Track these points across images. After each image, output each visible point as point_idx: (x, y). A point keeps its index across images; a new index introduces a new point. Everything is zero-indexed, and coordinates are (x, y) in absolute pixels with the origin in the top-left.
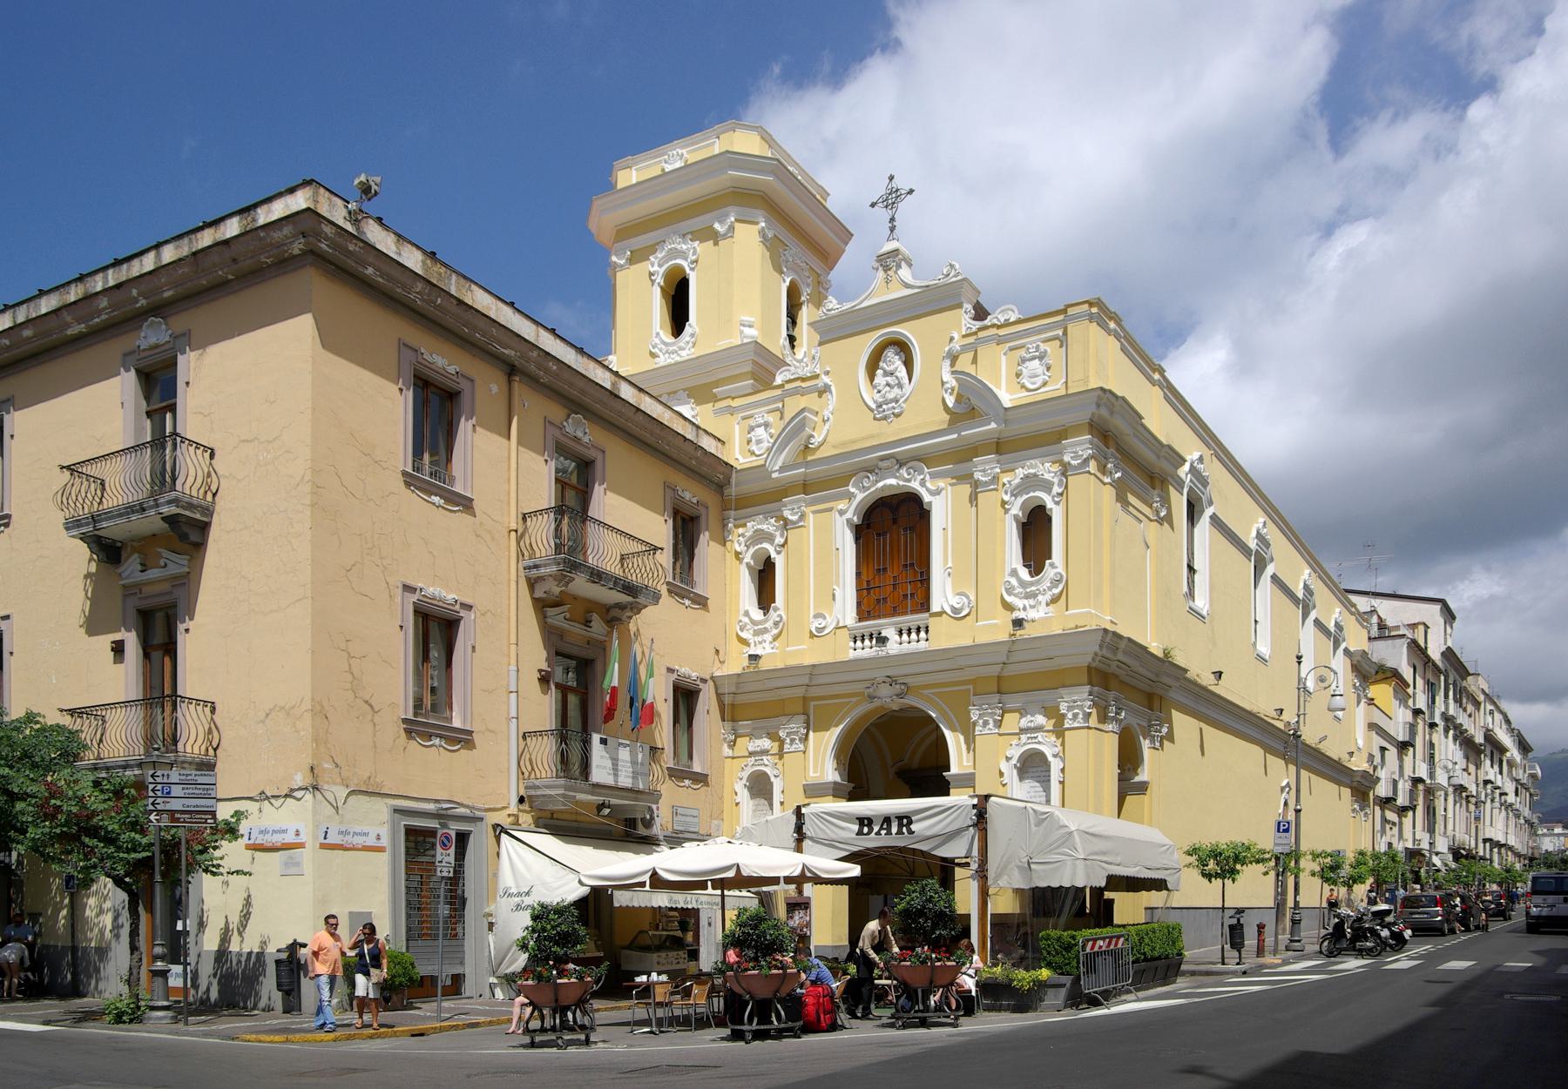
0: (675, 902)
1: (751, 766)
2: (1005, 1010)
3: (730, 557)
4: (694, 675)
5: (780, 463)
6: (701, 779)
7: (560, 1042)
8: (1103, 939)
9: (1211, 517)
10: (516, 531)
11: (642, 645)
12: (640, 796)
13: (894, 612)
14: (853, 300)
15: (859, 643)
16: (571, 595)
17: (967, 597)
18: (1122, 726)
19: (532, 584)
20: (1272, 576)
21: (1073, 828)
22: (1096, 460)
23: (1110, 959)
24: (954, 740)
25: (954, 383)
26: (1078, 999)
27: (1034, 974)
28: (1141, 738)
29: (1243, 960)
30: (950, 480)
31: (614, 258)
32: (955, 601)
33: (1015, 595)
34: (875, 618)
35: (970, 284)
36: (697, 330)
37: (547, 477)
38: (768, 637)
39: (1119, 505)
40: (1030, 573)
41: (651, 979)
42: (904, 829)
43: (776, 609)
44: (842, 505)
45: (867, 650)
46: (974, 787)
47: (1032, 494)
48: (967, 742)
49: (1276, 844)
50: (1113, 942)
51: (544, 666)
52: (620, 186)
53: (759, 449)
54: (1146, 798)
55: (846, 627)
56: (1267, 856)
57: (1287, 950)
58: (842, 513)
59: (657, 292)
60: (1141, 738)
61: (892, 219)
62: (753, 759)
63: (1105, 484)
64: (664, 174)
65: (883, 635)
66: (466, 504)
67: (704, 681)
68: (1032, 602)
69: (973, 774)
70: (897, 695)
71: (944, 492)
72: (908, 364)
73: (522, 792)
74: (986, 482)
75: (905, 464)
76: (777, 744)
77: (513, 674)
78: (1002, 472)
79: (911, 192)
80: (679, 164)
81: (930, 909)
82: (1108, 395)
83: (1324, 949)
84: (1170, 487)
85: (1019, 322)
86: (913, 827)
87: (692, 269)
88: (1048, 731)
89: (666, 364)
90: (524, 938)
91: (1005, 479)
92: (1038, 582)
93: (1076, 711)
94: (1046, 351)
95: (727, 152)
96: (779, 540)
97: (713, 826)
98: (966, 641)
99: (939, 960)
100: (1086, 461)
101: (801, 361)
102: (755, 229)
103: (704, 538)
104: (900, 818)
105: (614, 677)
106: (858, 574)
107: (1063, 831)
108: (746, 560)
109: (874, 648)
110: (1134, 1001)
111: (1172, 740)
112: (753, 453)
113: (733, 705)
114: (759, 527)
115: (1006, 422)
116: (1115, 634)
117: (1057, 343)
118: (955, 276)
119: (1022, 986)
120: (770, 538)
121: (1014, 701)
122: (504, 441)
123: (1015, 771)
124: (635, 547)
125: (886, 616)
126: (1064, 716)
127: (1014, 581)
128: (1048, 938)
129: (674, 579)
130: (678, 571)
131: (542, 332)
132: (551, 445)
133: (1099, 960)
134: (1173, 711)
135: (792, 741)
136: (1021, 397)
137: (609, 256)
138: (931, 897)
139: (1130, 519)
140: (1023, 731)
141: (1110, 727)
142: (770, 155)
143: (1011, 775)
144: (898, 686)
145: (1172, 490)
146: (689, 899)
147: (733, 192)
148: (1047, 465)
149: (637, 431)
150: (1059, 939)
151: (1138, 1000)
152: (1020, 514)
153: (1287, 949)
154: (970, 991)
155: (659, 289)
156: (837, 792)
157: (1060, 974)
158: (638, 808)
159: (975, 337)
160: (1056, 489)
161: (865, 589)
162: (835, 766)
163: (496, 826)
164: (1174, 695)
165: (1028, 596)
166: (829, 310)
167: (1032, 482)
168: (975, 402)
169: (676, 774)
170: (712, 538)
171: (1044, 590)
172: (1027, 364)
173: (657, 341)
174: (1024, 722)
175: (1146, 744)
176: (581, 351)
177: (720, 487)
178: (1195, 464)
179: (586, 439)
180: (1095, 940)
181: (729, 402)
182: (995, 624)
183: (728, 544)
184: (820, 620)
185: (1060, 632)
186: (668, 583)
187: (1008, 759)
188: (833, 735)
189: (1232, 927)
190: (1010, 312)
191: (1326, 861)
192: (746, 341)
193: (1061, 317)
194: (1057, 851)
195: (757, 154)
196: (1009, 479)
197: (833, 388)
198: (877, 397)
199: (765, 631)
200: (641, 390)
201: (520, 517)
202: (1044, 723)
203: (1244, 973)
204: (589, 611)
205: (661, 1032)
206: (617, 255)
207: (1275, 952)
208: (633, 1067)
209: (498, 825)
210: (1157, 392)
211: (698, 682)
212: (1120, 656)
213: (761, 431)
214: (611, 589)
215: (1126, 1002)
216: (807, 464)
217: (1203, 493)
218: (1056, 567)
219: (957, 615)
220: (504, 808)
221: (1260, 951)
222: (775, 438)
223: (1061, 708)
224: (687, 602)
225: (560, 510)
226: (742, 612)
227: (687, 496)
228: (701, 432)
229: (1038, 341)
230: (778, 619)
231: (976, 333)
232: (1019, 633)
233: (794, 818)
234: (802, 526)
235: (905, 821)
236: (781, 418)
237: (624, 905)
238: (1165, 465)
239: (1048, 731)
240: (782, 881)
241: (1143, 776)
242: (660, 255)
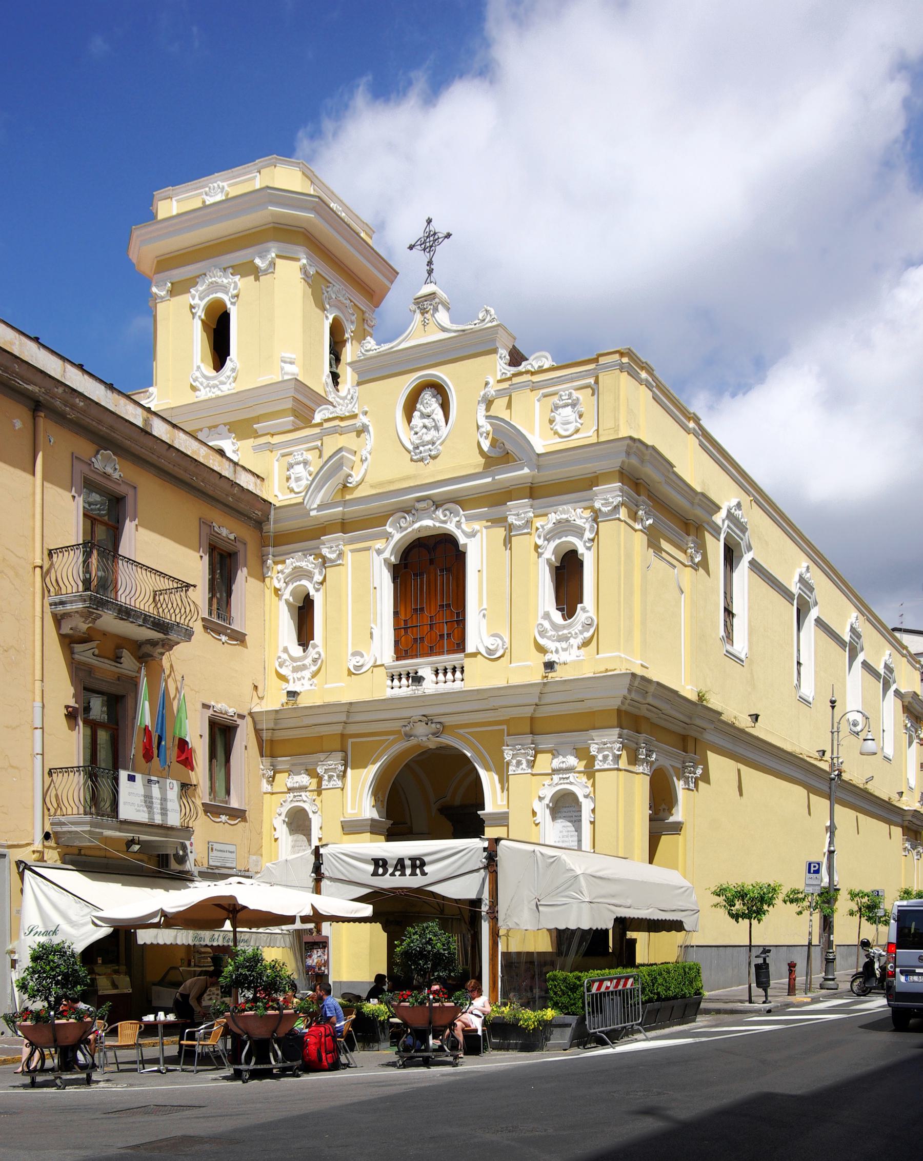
0: (200, 940)
1: (289, 803)
2: (513, 1049)
3: (269, 594)
4: (231, 711)
5: (318, 502)
6: (239, 815)
7: (58, 1081)
8: (611, 980)
9: (750, 562)
10: (41, 567)
11: (176, 681)
12: (170, 832)
13: (431, 652)
14: (390, 341)
15: (396, 682)
16: (99, 631)
17: (502, 639)
18: (654, 767)
19: (58, 620)
20: (816, 620)
21: (579, 872)
22: (626, 507)
23: (618, 999)
24: (488, 780)
25: (489, 428)
26: (582, 1039)
27: (539, 1013)
28: (675, 779)
29: (769, 999)
30: (484, 523)
31: (154, 290)
32: (491, 642)
33: (549, 638)
34: (412, 657)
35: (505, 329)
36: (238, 367)
37: (75, 512)
38: (307, 674)
39: (651, 550)
40: (563, 616)
41: (158, 1018)
42: (418, 871)
43: (315, 646)
44: (379, 544)
45: (404, 689)
46: (508, 826)
47: (564, 539)
48: (501, 782)
49: (807, 885)
50: (622, 983)
51: (72, 703)
52: (160, 216)
53: (299, 486)
54: (680, 838)
55: (383, 665)
56: (800, 896)
57: (821, 988)
58: (379, 552)
59: (198, 325)
60: (675, 779)
61: (430, 263)
62: (292, 795)
63: (636, 531)
64: (205, 206)
65: (419, 674)
66: (338, 390)
67: (242, 717)
68: (564, 645)
69: (507, 813)
70: (433, 734)
71: (479, 534)
72: (445, 406)
73: (48, 828)
74: (520, 526)
75: (441, 505)
76: (315, 781)
77: (38, 711)
78: (535, 516)
79: (448, 236)
80: (219, 197)
81: (429, 952)
82: (638, 444)
83: (855, 988)
84: (707, 534)
85: (552, 369)
86: (426, 869)
87: (233, 304)
88: (579, 772)
89: (206, 398)
90: (23, 979)
91: (538, 523)
92: (570, 626)
93: (606, 753)
94: (578, 399)
95: (268, 187)
96: (318, 578)
97: (251, 861)
98: (499, 682)
99: (437, 1001)
100: (616, 508)
101: (344, 398)
102: (296, 265)
103: (242, 574)
104: (413, 859)
105: (145, 715)
106: (396, 613)
107: (570, 874)
108: (285, 597)
109: (411, 687)
110: (644, 1040)
111: (708, 782)
112: (292, 491)
113: (272, 741)
114: (298, 564)
115: (539, 467)
116: (643, 678)
117: (589, 391)
118: (491, 321)
119: (528, 1025)
120: (309, 575)
121: (547, 742)
122: (29, 477)
123: (548, 811)
124: (166, 584)
125: (423, 655)
126: (594, 758)
127: (547, 624)
128: (554, 979)
129: (210, 614)
130: (215, 606)
131: (69, 367)
132: (79, 480)
133: (607, 1000)
134: (709, 753)
135: (330, 777)
136: (555, 444)
137: (150, 287)
138: (430, 939)
139: (663, 564)
140: (555, 771)
141: (640, 769)
142: (312, 192)
143: (544, 815)
144: (433, 725)
145: (707, 536)
146: (216, 936)
147: (274, 228)
148: (579, 511)
149: (169, 467)
150: (565, 980)
151: (647, 1039)
152: (553, 559)
153: (822, 987)
154: (476, 1030)
155: (200, 323)
156: (374, 828)
157: (566, 1014)
158: (169, 845)
159: (509, 383)
160: (588, 535)
161: (402, 628)
162: (373, 803)
163: (19, 863)
164: (710, 736)
165: (561, 639)
166: (367, 351)
167: (565, 527)
168: (509, 447)
169: (211, 810)
170: (250, 574)
171: (576, 634)
172: (560, 410)
173: (198, 374)
174: (557, 763)
175: (680, 785)
176: (110, 387)
177: (259, 524)
178: (733, 511)
179: (116, 475)
180: (601, 982)
181: (268, 439)
182: (527, 667)
183: (267, 580)
184: (358, 658)
185: (591, 675)
186: (203, 619)
187: (541, 799)
188: (370, 773)
189: (758, 967)
190: (544, 359)
191: (863, 900)
192: (286, 377)
193: (592, 366)
194: (563, 894)
195: (299, 190)
196: (542, 523)
197: (371, 429)
198: (415, 439)
199: (304, 668)
200: (174, 426)
201: (46, 553)
202: (576, 764)
203: (769, 1011)
204: (119, 647)
205: (168, 1071)
206: (157, 286)
207: (808, 989)
208: (119, 1107)
209: (22, 862)
210: (692, 440)
211: (235, 718)
212: (650, 700)
213: (299, 469)
214: (140, 625)
215: (637, 1041)
216: (345, 503)
217: (742, 539)
218: (587, 611)
219: (492, 656)
220: (28, 844)
221: (791, 990)
222: (313, 476)
223: (592, 749)
224: (224, 638)
225: (88, 547)
226: (281, 648)
227: (224, 532)
228: (238, 468)
229: (571, 388)
230: (317, 656)
231: (510, 379)
232: (550, 675)
233: (312, 859)
234: (339, 565)
235: (418, 862)
236: (320, 457)
237: (148, 942)
238: (699, 512)
239: (579, 772)
240: (298, 920)
241: (678, 815)
242: (201, 288)
